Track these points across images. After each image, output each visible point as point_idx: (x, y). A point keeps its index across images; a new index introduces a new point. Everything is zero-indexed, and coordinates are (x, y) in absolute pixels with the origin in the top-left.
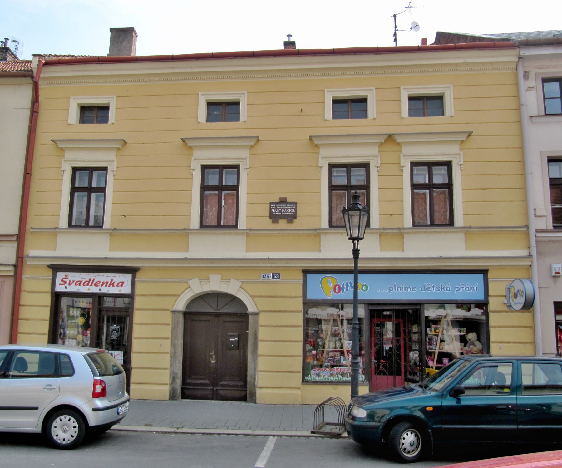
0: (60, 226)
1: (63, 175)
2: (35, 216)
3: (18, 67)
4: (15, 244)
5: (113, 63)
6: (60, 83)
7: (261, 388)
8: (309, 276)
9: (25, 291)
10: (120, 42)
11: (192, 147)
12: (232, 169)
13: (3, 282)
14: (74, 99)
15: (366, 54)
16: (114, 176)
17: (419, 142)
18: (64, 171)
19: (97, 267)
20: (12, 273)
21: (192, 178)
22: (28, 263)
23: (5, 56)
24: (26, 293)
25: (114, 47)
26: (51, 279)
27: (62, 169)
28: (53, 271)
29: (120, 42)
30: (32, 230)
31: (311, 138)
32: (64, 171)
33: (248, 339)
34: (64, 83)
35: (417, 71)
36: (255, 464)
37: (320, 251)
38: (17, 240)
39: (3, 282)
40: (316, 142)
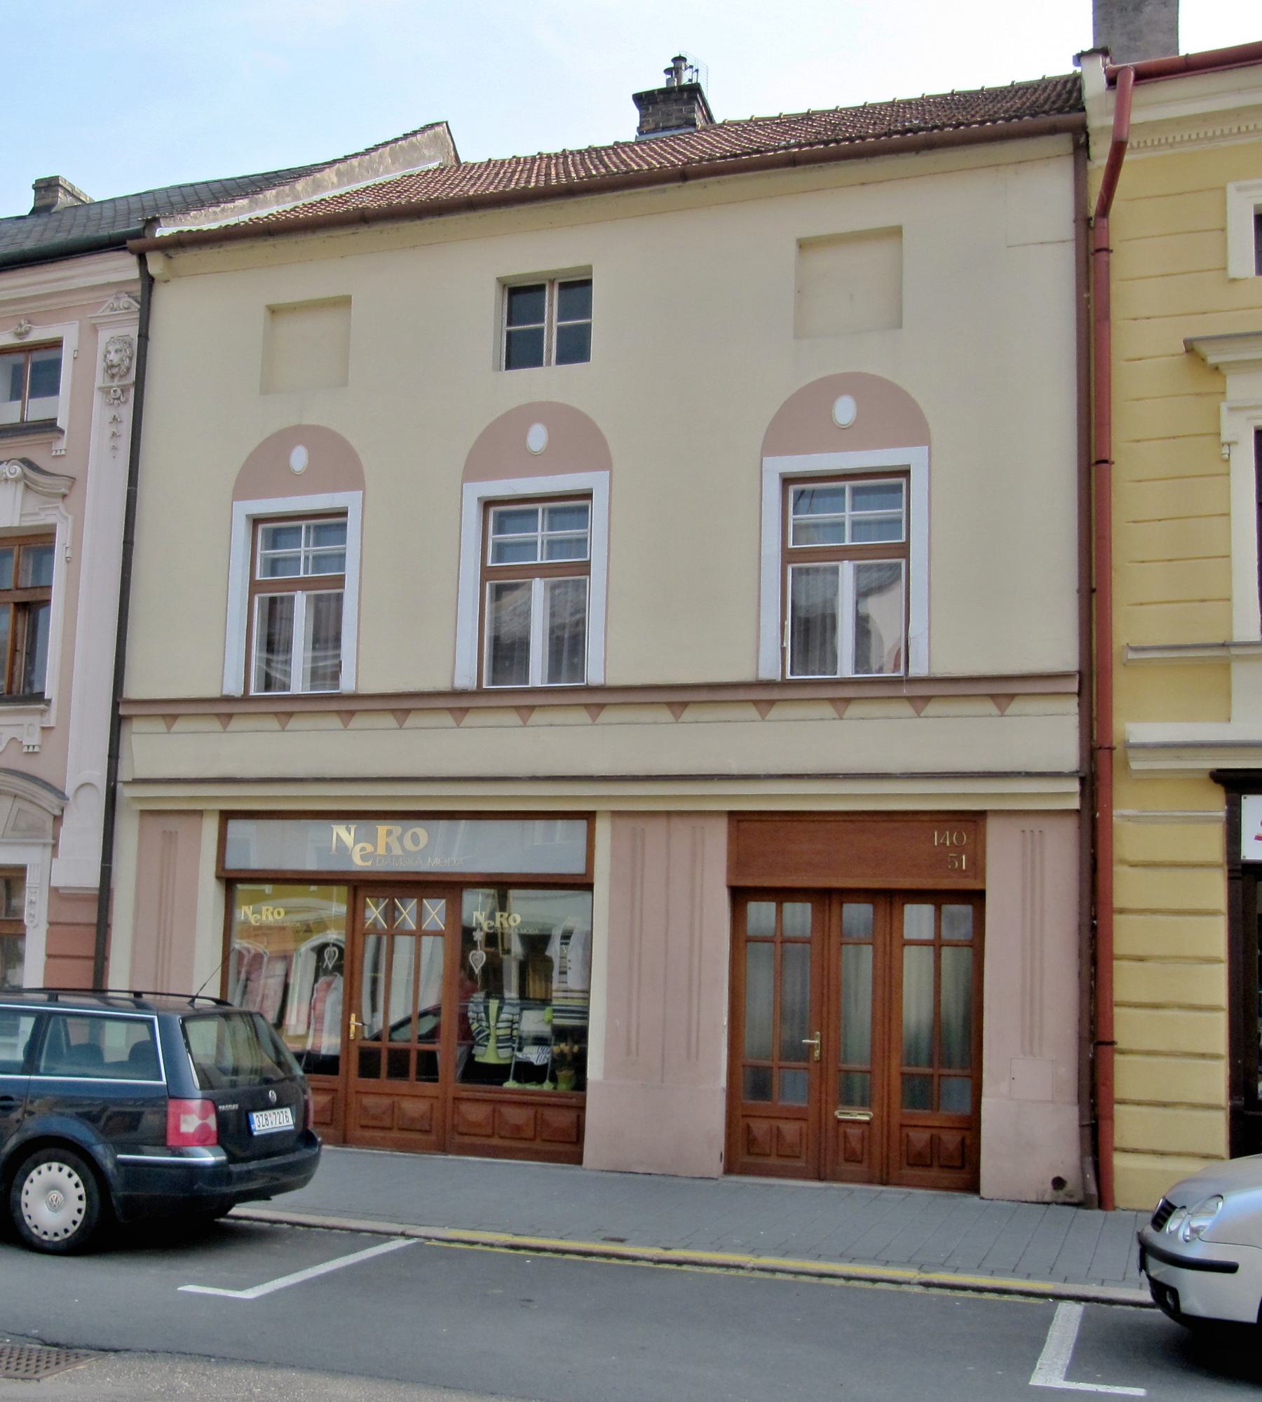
0: (1238, 637)
1: (1228, 461)
2: (1132, 605)
3: (721, 147)
4: (1072, 705)
5: (1206, 73)
6: (1182, 141)
7: (1125, 1151)
8: (234, 827)
9: (1123, 862)
10: (1130, 7)
11: (1221, 367)
12: (813, 482)
13: (1036, 833)
14: (1239, 189)
15: (1156, 82)
16: (68, 562)
17: (1246, 361)
18: (1229, 445)
19: (1231, 775)
20: (1075, 804)
21: (1228, 474)
22: (1134, 765)
23: (688, 112)
24: (1125, 869)
25: (1112, 27)
26: (1224, 820)
27: (1225, 437)
28: (1227, 792)
29: (1130, 7)
30: (1131, 655)
31: (1190, 347)
32: (1229, 445)
33: (729, 1003)
34: (1223, 135)
35: (1235, 130)
36: (1029, 1381)
37: (1230, 720)
38: (1079, 694)
39: (1036, 833)
40: (1212, 360)
